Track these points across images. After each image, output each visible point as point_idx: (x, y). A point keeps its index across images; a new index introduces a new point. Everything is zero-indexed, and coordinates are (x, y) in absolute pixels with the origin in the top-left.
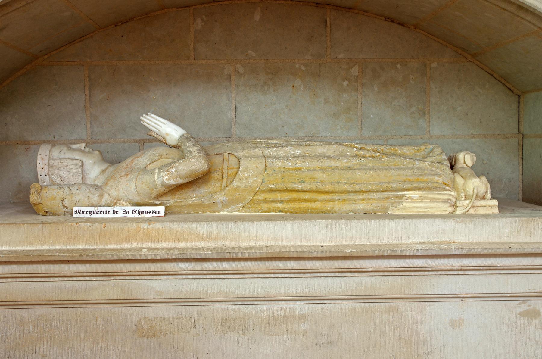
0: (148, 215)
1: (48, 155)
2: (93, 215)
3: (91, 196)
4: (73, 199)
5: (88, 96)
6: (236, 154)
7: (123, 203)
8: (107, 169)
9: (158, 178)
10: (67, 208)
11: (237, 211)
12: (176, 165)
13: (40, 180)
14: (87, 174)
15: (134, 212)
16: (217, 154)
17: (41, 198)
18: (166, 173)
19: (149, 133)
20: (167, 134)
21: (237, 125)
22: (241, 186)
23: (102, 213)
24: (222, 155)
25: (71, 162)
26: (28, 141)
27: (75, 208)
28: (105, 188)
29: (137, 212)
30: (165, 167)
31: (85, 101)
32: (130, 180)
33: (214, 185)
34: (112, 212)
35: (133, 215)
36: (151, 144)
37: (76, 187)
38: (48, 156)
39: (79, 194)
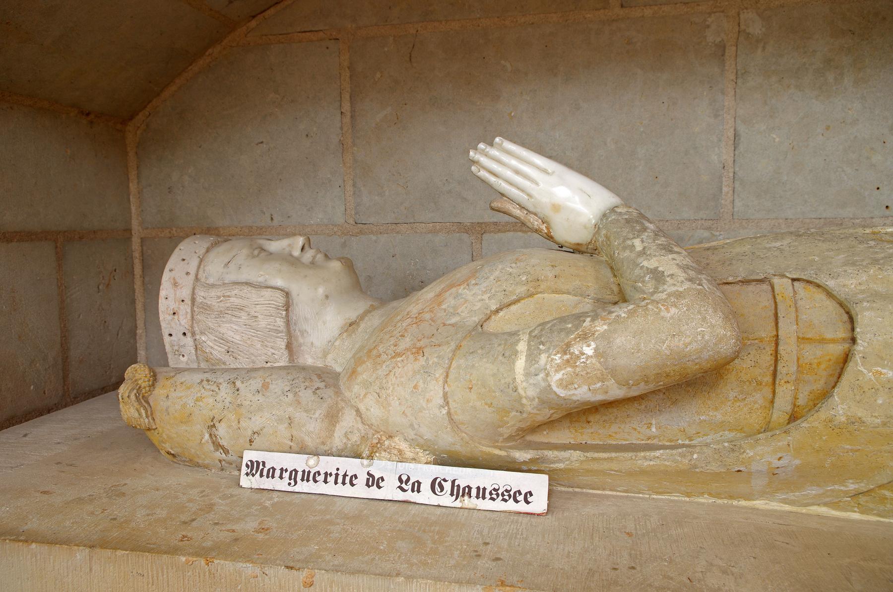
0: (486, 504)
1: (193, 272)
2: (303, 487)
3: (299, 416)
4: (243, 424)
5: (349, 114)
6: (831, 283)
7: (404, 446)
8: (362, 317)
9: (527, 375)
10: (226, 452)
11: (826, 504)
12: (601, 327)
13: (168, 348)
14: (303, 333)
15: (436, 485)
16: (746, 282)
17: (151, 415)
18: (557, 358)
19: (495, 205)
20: (556, 208)
21: (737, 184)
22: (869, 420)
23: (331, 479)
24: (765, 287)
25: (253, 295)
26: (217, 229)
27: (250, 455)
28: (349, 389)
29: (447, 486)
30: (558, 330)
31: (341, 128)
32: (426, 371)
33: (736, 399)
34: (362, 478)
35: (434, 500)
36: (500, 235)
37: (256, 384)
38: (192, 277)
39: (260, 409)
